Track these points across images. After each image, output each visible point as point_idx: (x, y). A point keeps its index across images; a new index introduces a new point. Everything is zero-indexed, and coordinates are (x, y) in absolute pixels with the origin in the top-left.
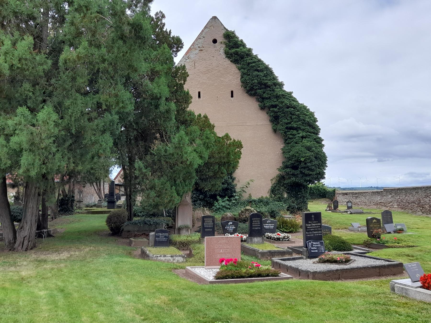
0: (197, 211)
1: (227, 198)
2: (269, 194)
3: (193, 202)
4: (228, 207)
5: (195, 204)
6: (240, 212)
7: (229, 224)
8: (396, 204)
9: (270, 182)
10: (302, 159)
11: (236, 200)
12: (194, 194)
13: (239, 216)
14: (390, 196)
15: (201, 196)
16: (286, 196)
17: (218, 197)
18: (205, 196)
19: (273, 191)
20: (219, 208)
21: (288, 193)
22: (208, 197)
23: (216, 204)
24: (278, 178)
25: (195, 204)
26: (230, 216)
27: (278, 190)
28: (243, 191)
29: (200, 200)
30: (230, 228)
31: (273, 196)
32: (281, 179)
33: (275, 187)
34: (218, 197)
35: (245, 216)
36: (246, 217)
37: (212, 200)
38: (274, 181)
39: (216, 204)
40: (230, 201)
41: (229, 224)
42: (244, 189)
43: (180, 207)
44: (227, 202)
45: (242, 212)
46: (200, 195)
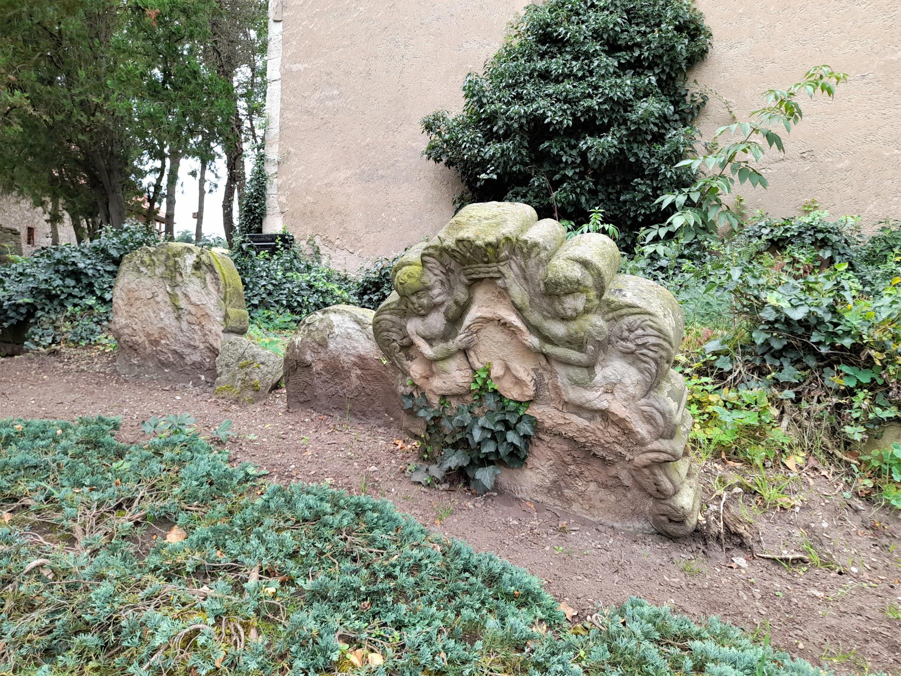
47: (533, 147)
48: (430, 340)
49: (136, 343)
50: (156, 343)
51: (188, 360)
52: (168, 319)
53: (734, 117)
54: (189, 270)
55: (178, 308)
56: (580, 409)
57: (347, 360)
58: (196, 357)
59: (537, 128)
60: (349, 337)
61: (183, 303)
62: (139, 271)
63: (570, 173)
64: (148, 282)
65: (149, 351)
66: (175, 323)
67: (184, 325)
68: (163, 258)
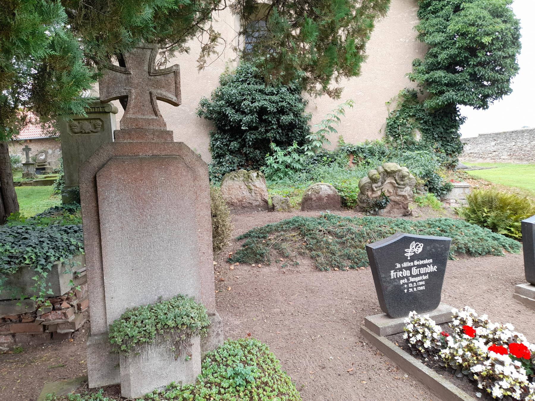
0: (228, 182)
1: (295, 146)
2: (383, 135)
3: (215, 158)
4: (298, 166)
5: (220, 163)
6: (366, 180)
7: (409, 253)
8: (505, 153)
9: (385, 108)
10: (486, 40)
11: (314, 149)
12: (216, 140)
13: (362, 193)
14: (493, 143)
15: (234, 145)
16: (418, 137)
17: (273, 145)
18: (243, 145)
19: (393, 129)
20: (278, 170)
21: (424, 131)
22: (249, 147)
23: (270, 160)
24: (402, 100)
25: (220, 163)
26: (330, 192)
27: (403, 125)
28: (331, 128)
29: (232, 152)
30: (415, 271)
31: (391, 139)
32: (410, 99)
33: (397, 118)
34: (273, 145)
35: (379, 193)
36: (383, 195)
37: (258, 152)
38: (394, 106)
39: (270, 160)
40: (301, 152)
41: (409, 253)
42: (332, 125)
43: (113, 171)
44: (295, 156)
45: (374, 180)
46: (230, 141)
47: (260, 117)
48: (376, 188)
49: (234, 202)
50: (241, 201)
51: (254, 205)
52: (246, 193)
53: (316, 108)
54: (255, 178)
55: (251, 189)
56: (400, 196)
57: (323, 196)
58: (257, 203)
59: (262, 111)
60: (326, 190)
61: (253, 188)
62: (234, 179)
63: (275, 127)
64: (237, 183)
65: (238, 204)
66: (249, 194)
67: (253, 194)
68: (242, 175)
